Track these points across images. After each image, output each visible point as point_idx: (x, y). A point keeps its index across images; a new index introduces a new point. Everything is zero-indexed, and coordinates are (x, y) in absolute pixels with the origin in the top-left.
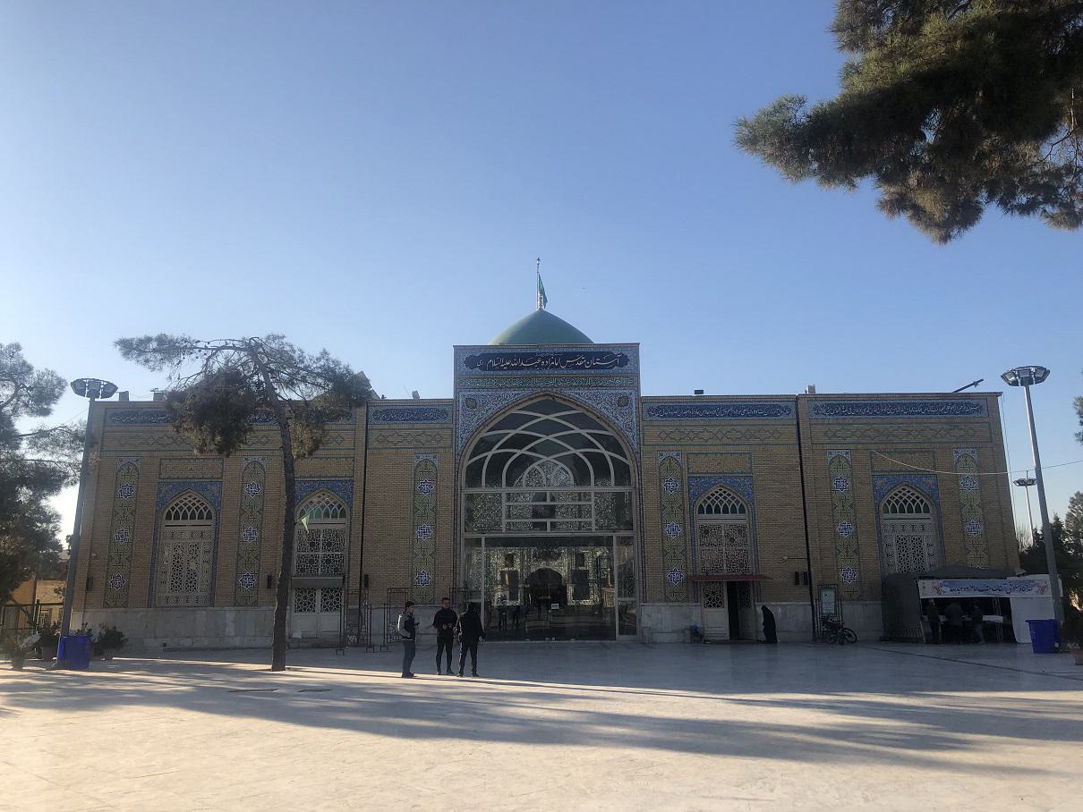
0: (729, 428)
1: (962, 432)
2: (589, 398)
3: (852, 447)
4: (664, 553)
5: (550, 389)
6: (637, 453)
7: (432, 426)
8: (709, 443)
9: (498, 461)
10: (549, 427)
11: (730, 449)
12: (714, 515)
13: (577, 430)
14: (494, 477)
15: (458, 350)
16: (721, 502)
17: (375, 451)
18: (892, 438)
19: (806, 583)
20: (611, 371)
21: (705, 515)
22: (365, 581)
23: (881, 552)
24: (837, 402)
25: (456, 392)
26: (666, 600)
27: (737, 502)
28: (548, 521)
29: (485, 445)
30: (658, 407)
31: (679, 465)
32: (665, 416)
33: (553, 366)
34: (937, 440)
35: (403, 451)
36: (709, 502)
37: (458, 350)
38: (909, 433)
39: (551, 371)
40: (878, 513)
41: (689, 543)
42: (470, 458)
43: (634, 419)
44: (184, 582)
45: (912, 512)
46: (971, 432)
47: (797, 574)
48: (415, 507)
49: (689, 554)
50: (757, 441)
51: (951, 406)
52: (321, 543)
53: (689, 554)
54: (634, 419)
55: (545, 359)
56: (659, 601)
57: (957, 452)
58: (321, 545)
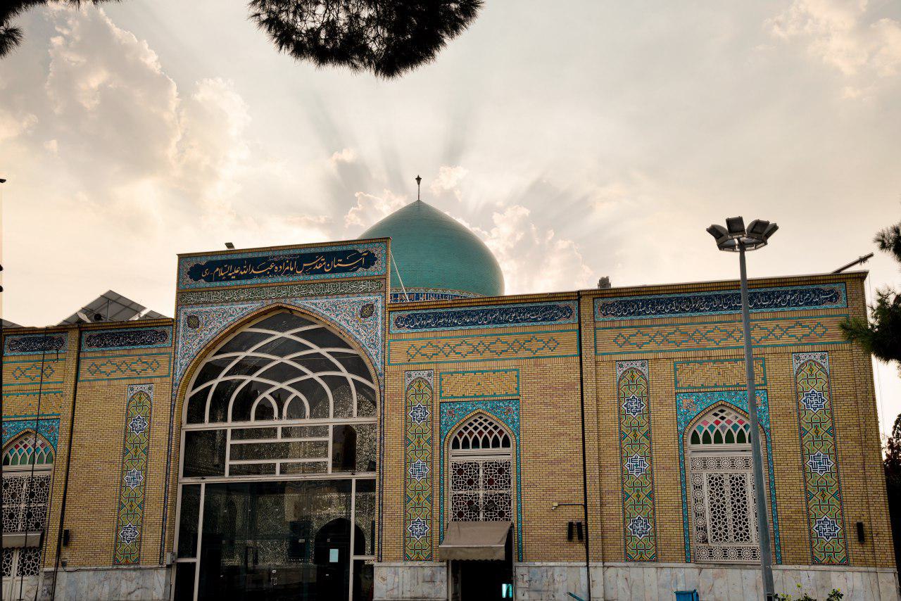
0: (494, 339)
1: (807, 331)
2: (327, 309)
3: (651, 356)
4: (407, 499)
5: (283, 301)
6: (381, 375)
7: (149, 351)
8: (468, 358)
9: (223, 392)
10: (284, 347)
11: (492, 365)
12: (471, 450)
13: (316, 349)
14: (218, 411)
15: (182, 258)
16: (481, 433)
17: (87, 384)
18: (704, 342)
19: (580, 537)
20: (354, 274)
21: (461, 451)
22: (65, 538)
23: (684, 496)
24: (633, 298)
25: (177, 311)
26: (406, 558)
27: (501, 432)
28: (278, 462)
29: (211, 371)
30: (409, 316)
31: (645, 379)
32: (416, 327)
33: (287, 272)
34: (769, 343)
35: (116, 382)
36: (718, 427)
37: (182, 258)
38: (730, 335)
39: (285, 279)
40: (682, 444)
41: (436, 487)
42: (194, 388)
43: (379, 334)
44: (730, 528)
45: (721, 442)
46: (820, 330)
47: (571, 524)
48: (125, 448)
49: (436, 500)
50: (528, 354)
51: (792, 295)
52: (481, 480)
53: (436, 500)
54: (379, 334)
55: (278, 263)
56: (396, 559)
57: (798, 358)
58: (481, 483)
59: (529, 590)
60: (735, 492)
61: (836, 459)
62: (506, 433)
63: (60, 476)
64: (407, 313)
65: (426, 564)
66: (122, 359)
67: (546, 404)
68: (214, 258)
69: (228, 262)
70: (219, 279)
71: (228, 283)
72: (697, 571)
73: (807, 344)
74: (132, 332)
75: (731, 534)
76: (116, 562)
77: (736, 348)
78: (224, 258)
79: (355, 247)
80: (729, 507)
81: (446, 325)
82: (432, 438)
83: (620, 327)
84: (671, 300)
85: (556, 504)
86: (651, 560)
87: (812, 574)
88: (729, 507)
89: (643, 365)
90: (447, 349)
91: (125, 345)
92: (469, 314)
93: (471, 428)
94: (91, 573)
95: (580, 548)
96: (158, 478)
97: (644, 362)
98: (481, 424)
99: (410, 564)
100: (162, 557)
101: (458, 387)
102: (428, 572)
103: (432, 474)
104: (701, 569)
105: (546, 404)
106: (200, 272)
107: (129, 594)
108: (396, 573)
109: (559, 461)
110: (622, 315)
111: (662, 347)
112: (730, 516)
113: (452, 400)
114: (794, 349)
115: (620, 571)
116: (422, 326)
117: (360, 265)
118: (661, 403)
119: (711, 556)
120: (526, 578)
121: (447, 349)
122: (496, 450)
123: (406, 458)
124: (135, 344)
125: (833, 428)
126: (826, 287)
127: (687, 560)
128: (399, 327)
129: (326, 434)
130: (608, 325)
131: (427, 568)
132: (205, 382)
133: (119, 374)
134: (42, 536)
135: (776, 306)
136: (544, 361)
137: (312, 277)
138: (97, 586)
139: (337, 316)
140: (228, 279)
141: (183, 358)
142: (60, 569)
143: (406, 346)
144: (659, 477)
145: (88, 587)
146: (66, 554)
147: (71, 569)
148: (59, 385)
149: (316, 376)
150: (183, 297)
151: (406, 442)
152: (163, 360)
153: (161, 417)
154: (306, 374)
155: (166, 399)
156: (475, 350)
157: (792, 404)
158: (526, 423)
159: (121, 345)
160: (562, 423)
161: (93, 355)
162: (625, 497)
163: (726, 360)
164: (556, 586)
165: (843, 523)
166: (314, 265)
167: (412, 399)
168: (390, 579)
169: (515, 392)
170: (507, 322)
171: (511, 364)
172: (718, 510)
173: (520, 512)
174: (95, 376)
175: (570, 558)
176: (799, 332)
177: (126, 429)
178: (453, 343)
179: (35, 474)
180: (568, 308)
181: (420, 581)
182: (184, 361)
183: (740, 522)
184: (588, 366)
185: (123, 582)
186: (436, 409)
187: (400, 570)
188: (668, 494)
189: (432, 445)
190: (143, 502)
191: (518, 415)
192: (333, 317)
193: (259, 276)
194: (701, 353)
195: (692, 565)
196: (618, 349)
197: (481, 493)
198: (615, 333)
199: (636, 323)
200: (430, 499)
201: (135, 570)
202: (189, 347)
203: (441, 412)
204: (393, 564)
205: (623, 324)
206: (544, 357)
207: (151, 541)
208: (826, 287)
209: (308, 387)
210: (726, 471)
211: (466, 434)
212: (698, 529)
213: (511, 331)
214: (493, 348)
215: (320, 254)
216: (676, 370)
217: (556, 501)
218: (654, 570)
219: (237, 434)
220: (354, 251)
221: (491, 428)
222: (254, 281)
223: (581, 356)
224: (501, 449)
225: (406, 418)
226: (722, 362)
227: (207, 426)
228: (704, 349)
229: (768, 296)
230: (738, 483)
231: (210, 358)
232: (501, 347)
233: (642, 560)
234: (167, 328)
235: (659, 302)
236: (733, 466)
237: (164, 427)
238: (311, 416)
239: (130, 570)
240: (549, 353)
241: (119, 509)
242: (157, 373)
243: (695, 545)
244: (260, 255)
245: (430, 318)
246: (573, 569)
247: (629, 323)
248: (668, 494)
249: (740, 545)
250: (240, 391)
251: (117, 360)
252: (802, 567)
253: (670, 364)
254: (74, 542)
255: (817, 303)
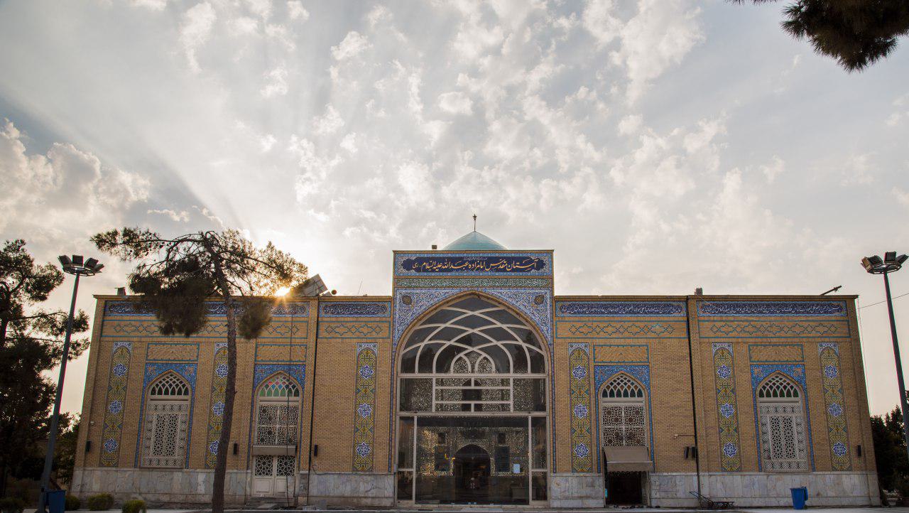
0: (631, 324)
3: (734, 340)
4: (573, 431)
9: (428, 353)
12: (615, 399)
14: (425, 366)
19: (693, 456)
20: (529, 274)
21: (609, 399)
22: (315, 451)
23: (757, 430)
26: (574, 470)
27: (636, 387)
28: (473, 403)
29: (419, 335)
32: (575, 313)
34: (805, 335)
42: (405, 348)
43: (549, 316)
45: (777, 396)
46: (833, 329)
49: (594, 430)
53: (594, 430)
54: (549, 316)
55: (472, 262)
57: (821, 345)
59: (659, 491)
60: (157, 442)
61: (844, 407)
62: (639, 387)
63: (308, 405)
64: (569, 303)
65: (587, 475)
66: (352, 324)
67: (667, 369)
68: (422, 256)
69: (433, 259)
70: (425, 270)
71: (433, 274)
72: (765, 477)
73: (826, 337)
74: (359, 305)
75: (784, 453)
76: (355, 469)
77: (785, 337)
78: (430, 256)
79: (529, 255)
80: (782, 436)
81: (596, 312)
82: (589, 390)
83: (714, 321)
84: (745, 305)
85: (676, 435)
86: (737, 471)
87: (832, 477)
88: (782, 436)
89: (729, 346)
90: (598, 330)
91: (353, 314)
92: (612, 307)
93: (615, 384)
94: (336, 476)
95: (693, 463)
96: (381, 408)
97: (730, 344)
98: (622, 381)
99: (576, 474)
100: (390, 466)
101: (606, 356)
102: (589, 480)
103: (590, 413)
104: (768, 476)
105: (667, 369)
106: (412, 265)
107: (366, 492)
108: (567, 481)
109: (677, 407)
110: (715, 313)
111: (741, 335)
112: (783, 443)
113: (603, 364)
114: (819, 340)
115: (719, 478)
116: (579, 313)
117: (532, 267)
118: (741, 371)
119: (773, 467)
120: (657, 483)
121: (598, 330)
122: (633, 399)
123: (571, 403)
124: (362, 313)
125: (842, 388)
126: (835, 303)
127: (760, 470)
128: (563, 312)
129: (508, 384)
130: (706, 319)
131: (589, 477)
132: (412, 345)
133: (349, 335)
134: (296, 448)
135: (808, 313)
136: (665, 341)
137: (497, 274)
138: (341, 486)
139: (517, 302)
140: (434, 271)
141: (400, 326)
142: (312, 472)
143: (568, 325)
144: (741, 418)
145: (334, 486)
146: (315, 461)
147: (321, 473)
148: (303, 340)
149: (499, 344)
150: (398, 282)
151: (571, 392)
152: (385, 326)
153: (384, 367)
154: (492, 342)
155: (388, 355)
156: (617, 331)
157: (819, 374)
158: (654, 382)
159: (351, 314)
160: (678, 382)
161: (329, 319)
162: (721, 430)
163: (779, 345)
164: (678, 488)
165: (848, 445)
166: (498, 266)
167: (573, 362)
168: (563, 485)
169: (646, 360)
170: (639, 313)
171: (642, 342)
172: (776, 439)
173: (652, 439)
174: (331, 335)
175: (685, 470)
176: (822, 329)
177: (357, 374)
178: (602, 325)
179: (290, 403)
180: (679, 306)
181: (584, 485)
182: (400, 328)
183: (264, 469)
184: (694, 345)
185: (361, 483)
186: (592, 370)
187: (570, 479)
188: (747, 428)
189: (590, 394)
190: (374, 428)
191: (649, 376)
192: (514, 302)
193: (457, 270)
194: (765, 340)
195: (763, 473)
196: (712, 335)
197: (624, 427)
198: (711, 325)
199: (724, 319)
200: (589, 431)
201: (369, 475)
202: (404, 317)
203: (595, 372)
204: (565, 475)
205: (715, 319)
206: (665, 338)
207: (381, 455)
208: (835, 303)
209: (518, 352)
210: (780, 415)
211: (160, 385)
212: (765, 451)
213: (642, 319)
214: (605, 330)
215: (503, 258)
216: (750, 350)
217: (676, 433)
218: (740, 477)
219: (441, 382)
220: (528, 258)
221: (178, 382)
222: (453, 273)
223: (689, 338)
224: (636, 398)
225: (570, 375)
226: (778, 346)
227: (417, 375)
228: (767, 337)
229: (803, 306)
230: (788, 422)
231: (418, 327)
232: (635, 329)
233: (732, 471)
234: (386, 304)
235: (738, 306)
236: (785, 411)
237: (386, 377)
238: (419, 372)
239: (366, 475)
240: (668, 335)
241: (355, 432)
242: (380, 336)
243: (765, 461)
244: (457, 256)
245: (585, 307)
246: (689, 477)
247: (719, 319)
248: (747, 428)
249: (790, 460)
250: (442, 352)
251: (348, 324)
252: (826, 473)
253: (746, 346)
254: (321, 453)
255: (830, 313)
